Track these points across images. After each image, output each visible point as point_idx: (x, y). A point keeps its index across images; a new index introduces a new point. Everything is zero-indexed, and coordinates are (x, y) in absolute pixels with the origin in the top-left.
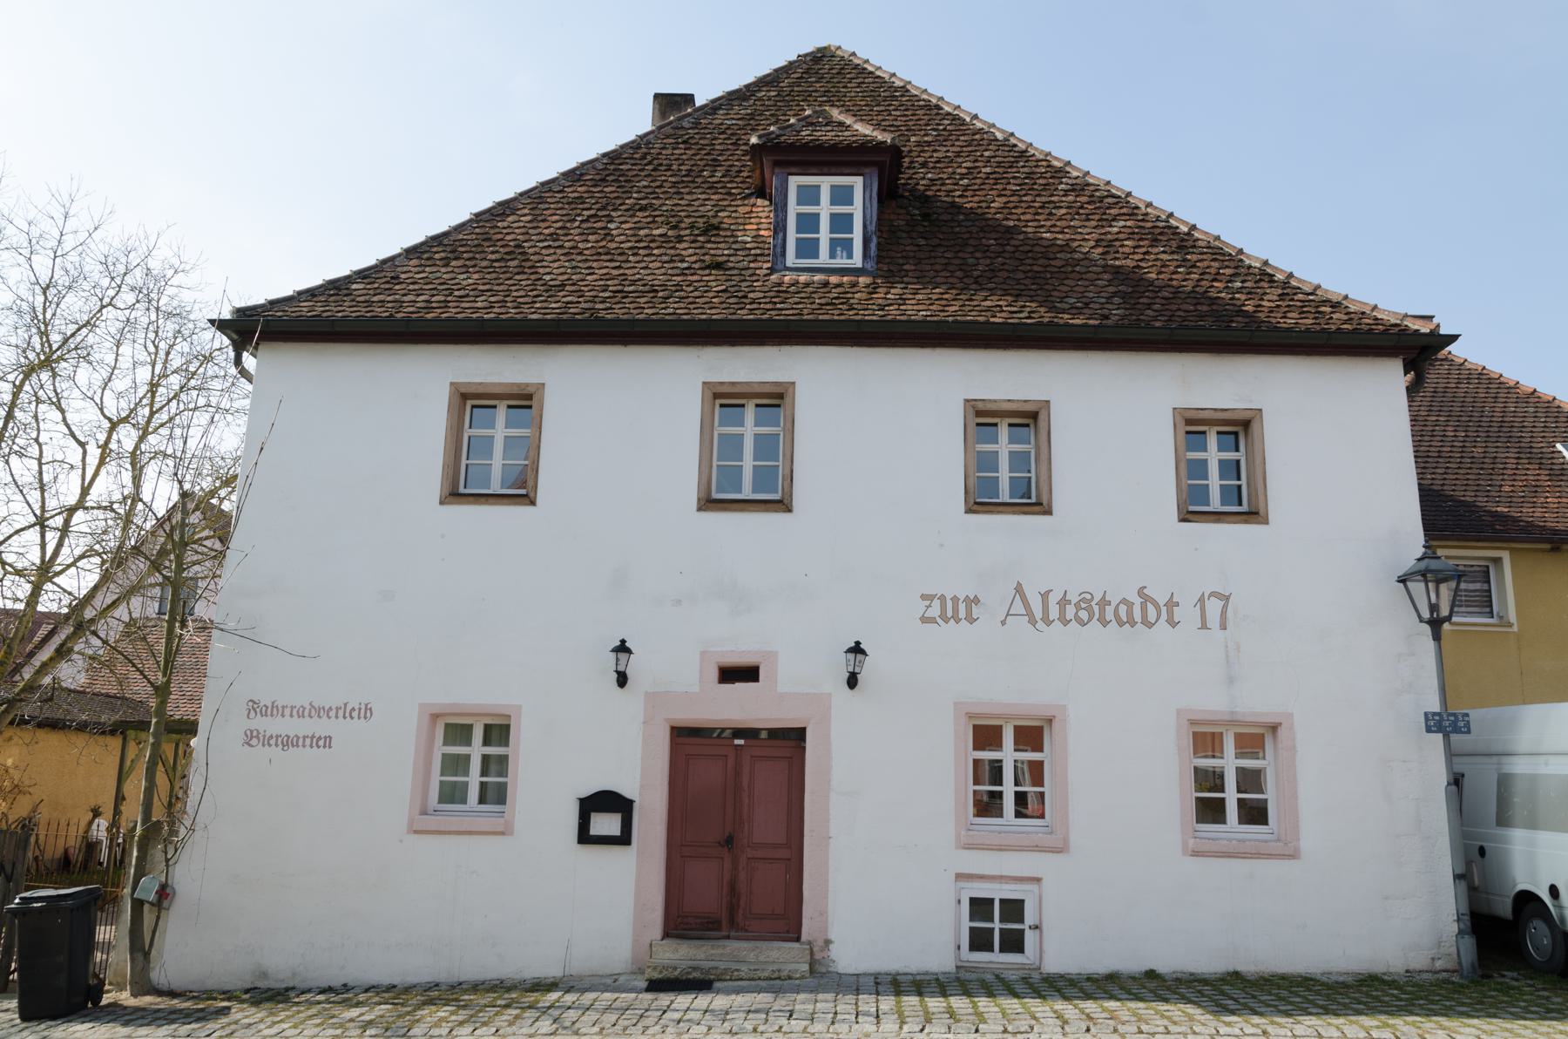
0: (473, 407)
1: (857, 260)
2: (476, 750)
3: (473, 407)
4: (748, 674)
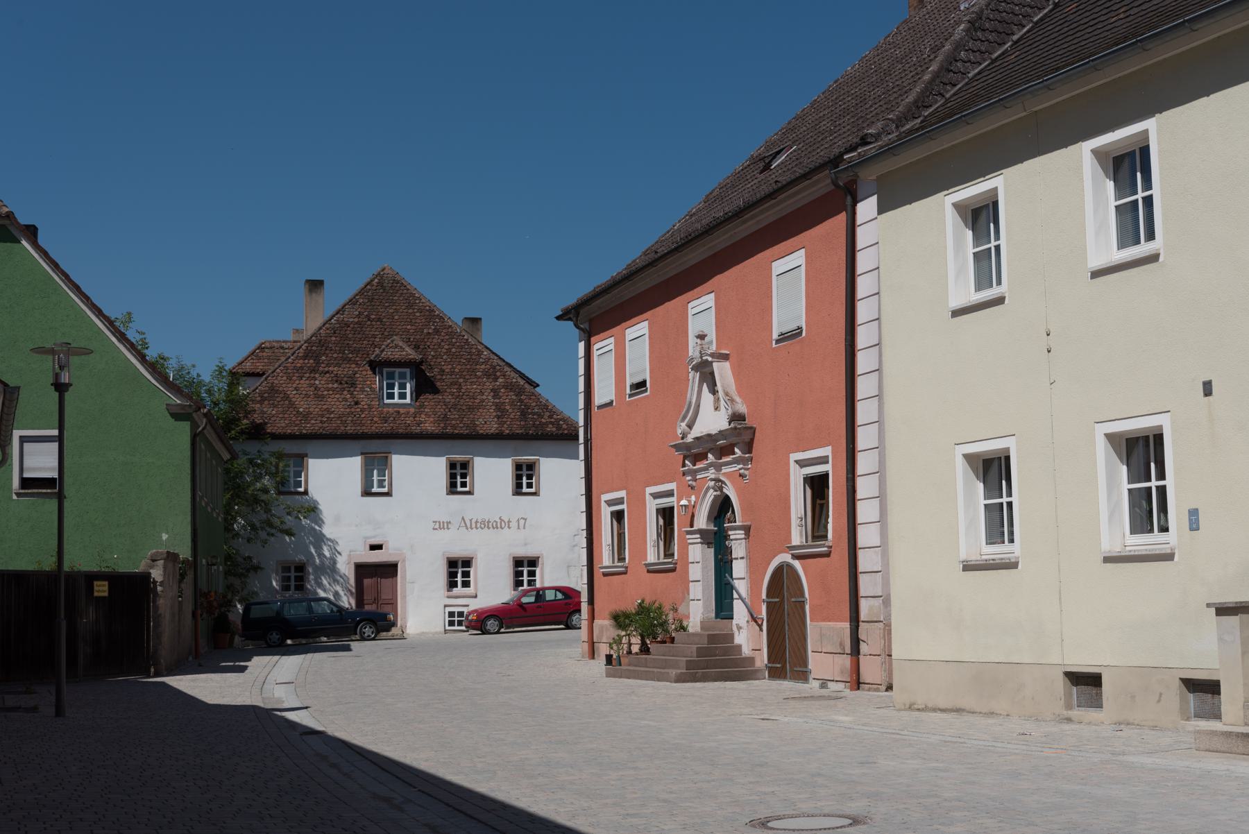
0: (23, 439)
1: (408, 400)
2: (293, 574)
3: (23, 439)
4: (379, 547)
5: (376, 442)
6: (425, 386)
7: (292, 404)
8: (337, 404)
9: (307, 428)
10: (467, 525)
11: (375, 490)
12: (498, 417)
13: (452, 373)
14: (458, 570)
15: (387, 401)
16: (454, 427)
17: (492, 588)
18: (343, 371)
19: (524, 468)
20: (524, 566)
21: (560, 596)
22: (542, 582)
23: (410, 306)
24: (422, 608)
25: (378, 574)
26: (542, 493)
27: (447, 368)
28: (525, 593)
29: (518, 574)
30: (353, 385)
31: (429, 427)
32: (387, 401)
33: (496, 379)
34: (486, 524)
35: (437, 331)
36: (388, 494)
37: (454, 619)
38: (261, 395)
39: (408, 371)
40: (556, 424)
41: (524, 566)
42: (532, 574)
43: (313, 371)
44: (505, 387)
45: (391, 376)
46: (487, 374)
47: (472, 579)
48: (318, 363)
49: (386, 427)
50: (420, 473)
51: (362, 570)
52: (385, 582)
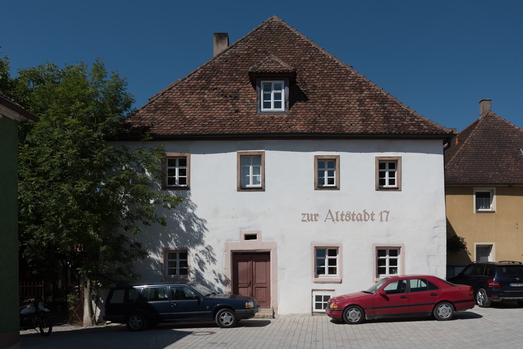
1: (283, 109)
4: (253, 237)
5: (250, 139)
6: (296, 96)
7: (181, 113)
8: (220, 112)
9: (189, 130)
10: (334, 217)
11: (251, 185)
12: (363, 121)
13: (323, 88)
14: (325, 258)
15: (263, 110)
16: (322, 128)
17: (357, 278)
18: (232, 87)
19: (387, 166)
20: (386, 256)
21: (424, 285)
22: (403, 270)
23: (292, 42)
24: (292, 292)
25: (251, 261)
26: (403, 188)
27: (319, 85)
28: (389, 281)
29: (381, 262)
30: (236, 98)
31: (299, 128)
32: (263, 110)
33: (362, 91)
34: (350, 217)
35: (312, 59)
36: (262, 189)
37: (321, 302)
38: (156, 106)
39: (282, 82)
40: (418, 125)
41: (386, 256)
42: (394, 262)
43: (204, 88)
44: (370, 97)
45: (268, 89)
46: (354, 88)
47: (338, 266)
48: (209, 82)
49: (260, 129)
50: (289, 167)
51: (238, 257)
52: (260, 265)
